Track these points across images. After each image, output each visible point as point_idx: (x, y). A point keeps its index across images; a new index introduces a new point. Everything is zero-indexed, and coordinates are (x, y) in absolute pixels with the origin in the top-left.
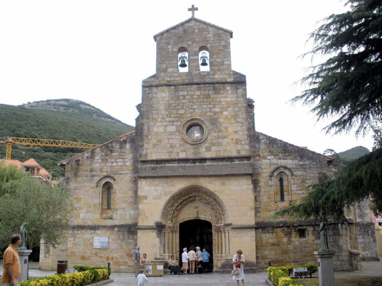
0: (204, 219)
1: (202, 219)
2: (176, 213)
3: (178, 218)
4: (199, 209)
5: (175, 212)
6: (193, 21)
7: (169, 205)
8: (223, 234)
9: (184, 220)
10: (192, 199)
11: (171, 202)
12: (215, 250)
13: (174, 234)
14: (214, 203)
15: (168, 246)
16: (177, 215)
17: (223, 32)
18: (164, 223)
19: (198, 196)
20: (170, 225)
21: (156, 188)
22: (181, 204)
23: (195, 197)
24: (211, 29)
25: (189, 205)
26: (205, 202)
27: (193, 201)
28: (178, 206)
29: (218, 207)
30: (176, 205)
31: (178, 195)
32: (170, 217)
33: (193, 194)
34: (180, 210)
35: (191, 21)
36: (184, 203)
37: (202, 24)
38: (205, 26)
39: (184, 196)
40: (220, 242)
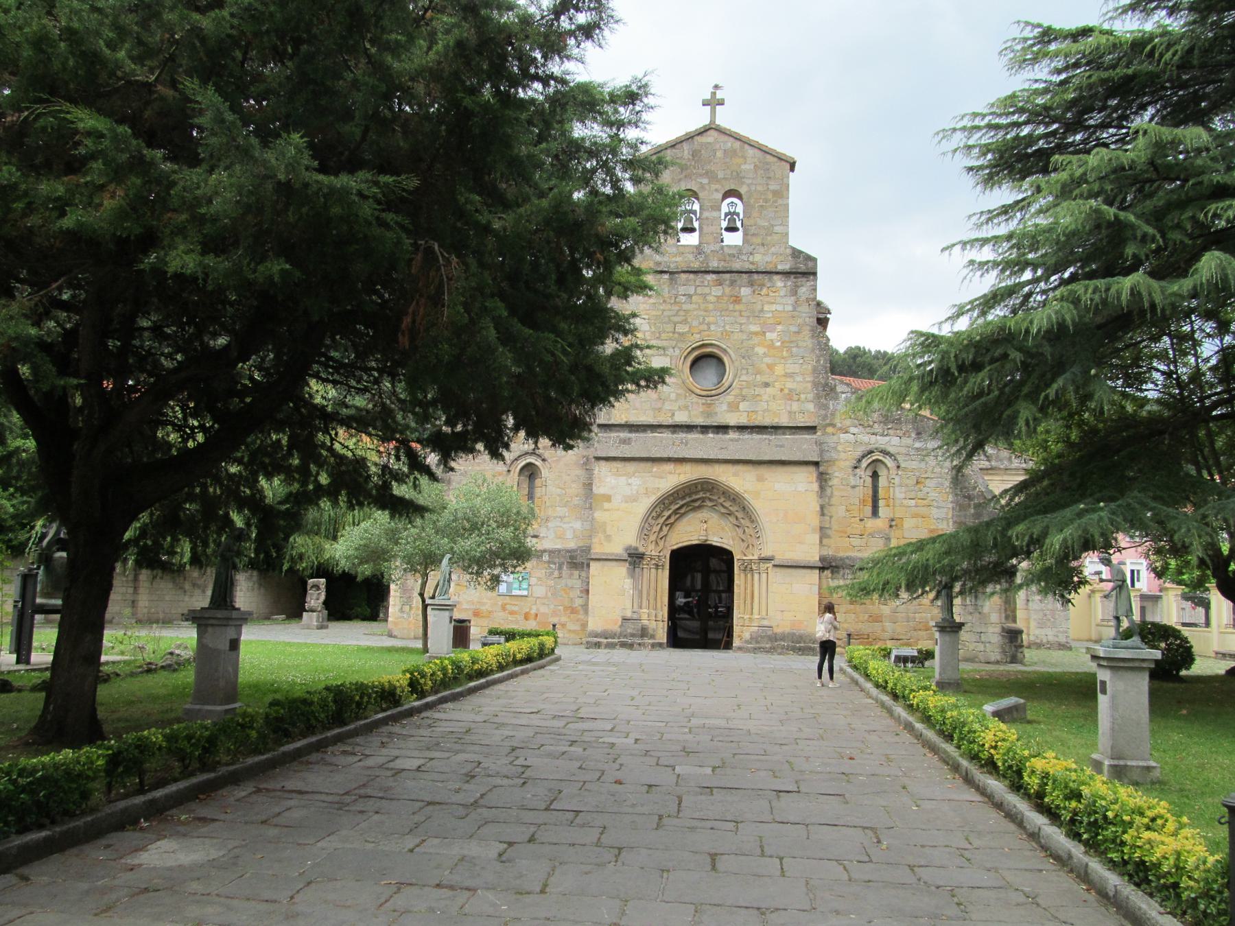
0: (718, 545)
1: (714, 544)
2: (665, 529)
3: (668, 539)
4: (710, 522)
5: (664, 527)
6: (712, 132)
7: (654, 514)
8: (756, 576)
9: (680, 545)
10: (697, 504)
11: (658, 509)
12: (739, 607)
13: (660, 571)
14: (740, 515)
15: (648, 594)
16: (666, 536)
17: (776, 159)
18: (641, 550)
19: (710, 500)
20: (653, 553)
21: (630, 481)
22: (675, 512)
23: (703, 499)
24: (750, 152)
25: (691, 516)
26: (723, 510)
27: (699, 507)
28: (669, 517)
29: (748, 524)
30: (667, 514)
31: (672, 495)
32: (653, 537)
33: (701, 495)
34: (672, 524)
35: (709, 133)
36: (682, 511)
37: (731, 139)
38: (737, 144)
39: (683, 498)
40: (749, 591)
